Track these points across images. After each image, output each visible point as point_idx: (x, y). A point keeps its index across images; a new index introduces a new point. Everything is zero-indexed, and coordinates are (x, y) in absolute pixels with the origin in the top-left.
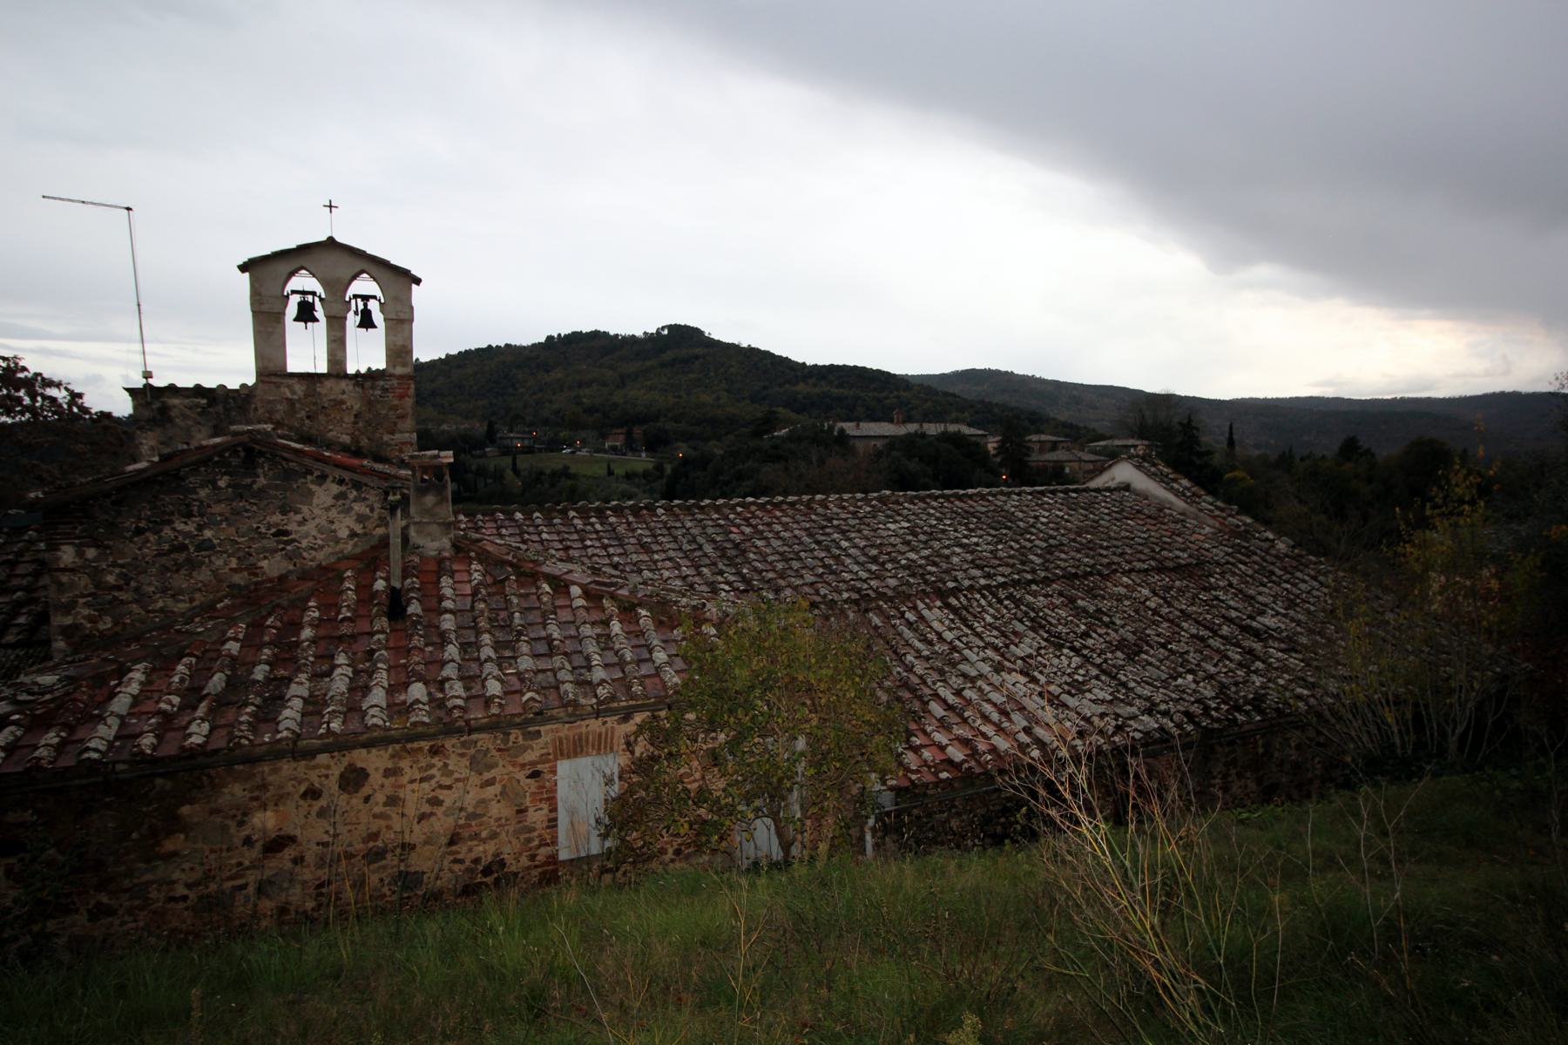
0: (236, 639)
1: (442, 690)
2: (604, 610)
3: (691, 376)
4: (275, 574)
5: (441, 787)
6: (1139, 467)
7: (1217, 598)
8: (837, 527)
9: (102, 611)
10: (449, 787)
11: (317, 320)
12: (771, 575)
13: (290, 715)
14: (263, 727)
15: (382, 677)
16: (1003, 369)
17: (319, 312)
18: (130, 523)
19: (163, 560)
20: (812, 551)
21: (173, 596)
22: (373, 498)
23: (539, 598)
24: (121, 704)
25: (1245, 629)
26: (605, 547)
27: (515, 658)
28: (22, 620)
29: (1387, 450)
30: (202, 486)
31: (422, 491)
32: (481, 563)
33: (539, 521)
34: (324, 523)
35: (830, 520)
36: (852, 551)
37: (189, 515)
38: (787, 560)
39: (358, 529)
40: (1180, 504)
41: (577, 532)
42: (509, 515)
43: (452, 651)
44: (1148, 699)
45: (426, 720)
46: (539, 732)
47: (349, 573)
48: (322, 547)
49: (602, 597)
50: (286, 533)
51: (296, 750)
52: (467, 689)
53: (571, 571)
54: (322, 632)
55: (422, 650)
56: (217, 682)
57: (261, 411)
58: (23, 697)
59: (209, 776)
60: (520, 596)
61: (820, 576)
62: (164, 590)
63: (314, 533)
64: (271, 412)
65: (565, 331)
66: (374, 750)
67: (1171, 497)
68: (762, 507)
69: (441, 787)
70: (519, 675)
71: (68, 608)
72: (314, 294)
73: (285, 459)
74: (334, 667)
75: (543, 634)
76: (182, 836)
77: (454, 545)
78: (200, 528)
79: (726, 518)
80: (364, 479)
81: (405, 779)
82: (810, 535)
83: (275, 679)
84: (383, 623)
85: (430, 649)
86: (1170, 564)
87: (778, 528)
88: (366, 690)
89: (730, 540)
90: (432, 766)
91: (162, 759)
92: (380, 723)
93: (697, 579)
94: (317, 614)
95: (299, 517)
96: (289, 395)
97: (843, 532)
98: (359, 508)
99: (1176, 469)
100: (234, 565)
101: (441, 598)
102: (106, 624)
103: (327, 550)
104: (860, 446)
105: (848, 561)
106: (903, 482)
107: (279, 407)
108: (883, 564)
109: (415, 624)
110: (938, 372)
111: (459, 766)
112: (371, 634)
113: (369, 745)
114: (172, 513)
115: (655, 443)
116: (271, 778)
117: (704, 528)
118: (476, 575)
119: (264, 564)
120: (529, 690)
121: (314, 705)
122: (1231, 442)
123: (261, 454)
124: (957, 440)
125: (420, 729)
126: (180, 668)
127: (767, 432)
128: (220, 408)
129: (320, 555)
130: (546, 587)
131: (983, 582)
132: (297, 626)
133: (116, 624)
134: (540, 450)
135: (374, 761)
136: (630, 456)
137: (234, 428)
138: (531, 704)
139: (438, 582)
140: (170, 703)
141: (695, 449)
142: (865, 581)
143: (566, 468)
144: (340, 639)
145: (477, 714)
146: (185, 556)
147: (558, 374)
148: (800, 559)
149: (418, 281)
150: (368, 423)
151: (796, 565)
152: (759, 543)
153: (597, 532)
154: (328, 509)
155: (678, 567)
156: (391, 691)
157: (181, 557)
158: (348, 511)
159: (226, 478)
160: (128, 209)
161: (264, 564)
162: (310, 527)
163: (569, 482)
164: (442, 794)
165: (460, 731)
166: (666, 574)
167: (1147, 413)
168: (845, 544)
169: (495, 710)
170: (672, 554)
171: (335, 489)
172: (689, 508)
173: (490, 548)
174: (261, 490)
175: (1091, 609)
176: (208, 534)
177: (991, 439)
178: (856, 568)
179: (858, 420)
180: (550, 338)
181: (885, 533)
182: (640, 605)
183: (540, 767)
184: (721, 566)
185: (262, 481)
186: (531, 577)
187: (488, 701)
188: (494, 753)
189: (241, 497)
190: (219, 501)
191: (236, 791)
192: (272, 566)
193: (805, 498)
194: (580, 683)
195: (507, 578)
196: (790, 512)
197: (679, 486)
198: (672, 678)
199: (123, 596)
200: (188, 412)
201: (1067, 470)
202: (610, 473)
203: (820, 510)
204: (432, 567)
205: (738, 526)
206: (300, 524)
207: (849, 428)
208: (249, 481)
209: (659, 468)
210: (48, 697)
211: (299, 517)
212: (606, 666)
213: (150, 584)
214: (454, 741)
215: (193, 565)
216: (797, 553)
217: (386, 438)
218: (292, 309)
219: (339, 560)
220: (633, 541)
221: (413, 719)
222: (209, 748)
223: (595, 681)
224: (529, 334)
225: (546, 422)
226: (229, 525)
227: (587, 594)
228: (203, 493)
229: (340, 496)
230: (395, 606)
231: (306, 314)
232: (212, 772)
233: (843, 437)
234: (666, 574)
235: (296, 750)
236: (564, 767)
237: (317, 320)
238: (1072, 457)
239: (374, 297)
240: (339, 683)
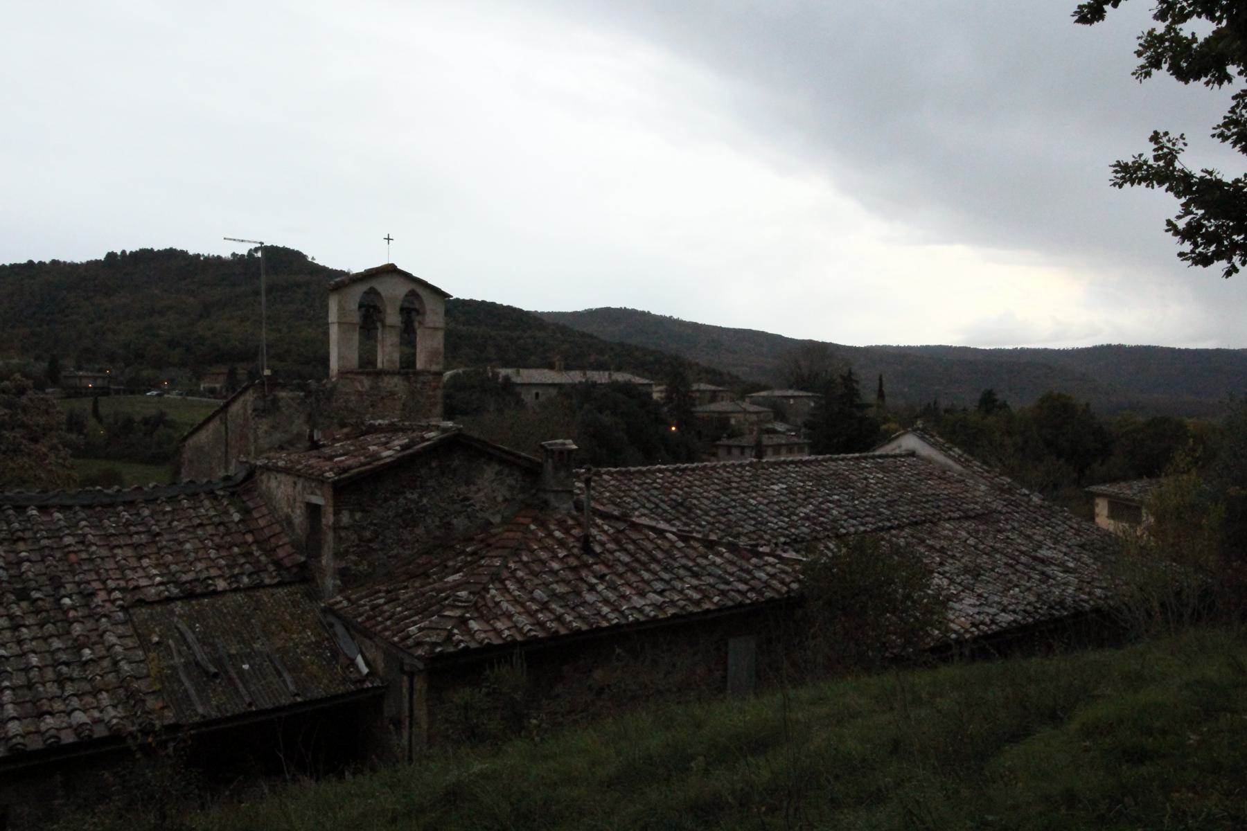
6: (922, 438)
7: (1008, 538)
16: (640, 308)
25: (1035, 558)
29: (1021, 403)
39: (508, 496)
40: (958, 467)
44: (999, 603)
50: (467, 499)
65: (132, 247)
67: (950, 462)
78: (420, 497)
86: (972, 514)
99: (950, 440)
104: (528, 397)
119: (455, 521)
122: (881, 394)
124: (627, 389)
128: (313, 399)
131: (862, 528)
143: (162, 414)
167: (802, 363)
175: (938, 546)
177: (655, 389)
180: (111, 256)
201: (733, 421)
224: (83, 248)
233: (508, 385)
238: (738, 409)
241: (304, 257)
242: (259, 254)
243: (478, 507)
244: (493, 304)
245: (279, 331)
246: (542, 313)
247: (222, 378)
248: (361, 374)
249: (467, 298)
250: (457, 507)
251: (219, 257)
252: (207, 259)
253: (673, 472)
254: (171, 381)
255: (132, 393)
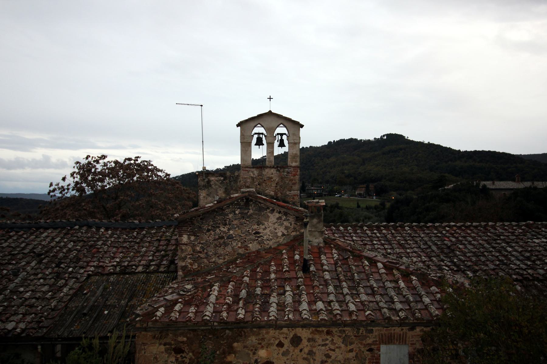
0: (247, 276)
1: (330, 306)
2: (394, 275)
3: (399, 159)
4: (254, 250)
5: (331, 350)
8: (504, 240)
9: (195, 261)
10: (334, 350)
11: (263, 145)
12: (469, 263)
13: (273, 309)
14: (263, 314)
15: (304, 297)
17: (264, 142)
18: (205, 227)
19: (216, 242)
20: (491, 252)
21: (218, 257)
22: (292, 219)
23: (363, 267)
24: (212, 299)
26: (383, 245)
27: (359, 295)
28: (164, 262)
30: (230, 213)
31: (312, 217)
32: (336, 250)
33: (351, 231)
34: (273, 229)
35: (499, 236)
36: (514, 253)
37: (225, 225)
38: (477, 256)
39: (285, 232)
41: (369, 237)
42: (337, 228)
43: (331, 288)
45: (326, 318)
46: (372, 330)
47: (284, 251)
48: (271, 240)
49: (392, 269)
50: (259, 233)
51: (276, 326)
52: (341, 306)
53: (377, 256)
54: (278, 276)
55: (318, 287)
56: (243, 293)
57: (242, 182)
58: (182, 293)
59: (244, 332)
60: (355, 266)
61: (498, 265)
62: (215, 254)
63: (269, 233)
64: (245, 182)
65: (337, 139)
66: (304, 329)
68: (459, 228)
69: (331, 350)
70: (362, 302)
71: (184, 259)
72: (262, 134)
73: (260, 203)
74: (285, 291)
75: (368, 284)
76: (234, 355)
77: (324, 241)
78: (229, 230)
79: (441, 233)
80: (289, 212)
81: (317, 344)
82: (489, 243)
83: (264, 294)
84: (300, 274)
85: (321, 287)
87: (470, 239)
88: (300, 303)
89: (445, 244)
90: (327, 339)
91: (229, 322)
92: (308, 317)
93: (430, 263)
94: (275, 268)
95: (263, 227)
96: (252, 175)
97: (507, 243)
98: (286, 223)
100: (240, 246)
101: (323, 265)
102: (195, 266)
103: (273, 241)
105: (513, 259)
106: (521, 215)
107: (248, 180)
108: (534, 261)
109: (314, 275)
110: (541, 153)
111: (339, 341)
112: (297, 278)
113: (304, 326)
114: (220, 224)
115: (380, 192)
116: (266, 336)
117: (430, 237)
118: (335, 255)
119: (250, 245)
120: (368, 310)
121: (281, 307)
123: (251, 200)
125: (323, 322)
126: (230, 286)
127: (440, 187)
128: (228, 181)
129: (271, 243)
130: (366, 263)
132: (268, 272)
133: (199, 267)
134: (325, 195)
135: (304, 334)
136: (368, 198)
137: (242, 190)
138: (370, 316)
139: (320, 258)
140: (229, 300)
141: (400, 195)
142: (525, 270)
143: (337, 204)
144: (286, 279)
145: (347, 318)
146: (223, 241)
147: (333, 159)
148: (484, 256)
149: (302, 126)
150: (281, 187)
151: (483, 259)
152: (461, 246)
153: (378, 237)
154: (274, 224)
155: (420, 256)
156: (310, 303)
157: (222, 241)
158: (282, 225)
159: (239, 210)
160: (202, 106)
161: (250, 245)
162: (267, 231)
163: (340, 211)
164: (331, 353)
165: (339, 325)
166: (415, 259)
168: (509, 249)
169: (354, 317)
170: (416, 249)
171: (278, 215)
172: (421, 227)
173: (339, 243)
174: (251, 215)
176: (231, 232)
178: (518, 263)
179: (492, 180)
180: (330, 143)
181: (533, 245)
182: (412, 273)
183: (373, 347)
184: (442, 257)
185: (251, 211)
186: (359, 257)
187: (351, 313)
188: (353, 337)
189: (243, 218)
190: (236, 219)
191: (253, 340)
192: (253, 247)
193: (483, 224)
194: (390, 309)
195: (349, 257)
196: (475, 231)
197: (394, 215)
198: (434, 311)
199: (202, 255)
200: (217, 183)
202: (359, 206)
203: (492, 230)
204: (316, 250)
205: (448, 237)
206: (264, 229)
207: (489, 184)
208: (246, 211)
209: (383, 204)
210: (189, 293)
211: (263, 227)
212: (401, 302)
213: (211, 251)
214: (336, 329)
215: (226, 244)
216: (483, 253)
217: (288, 193)
218: (254, 141)
219: (278, 245)
220: (395, 242)
221: (321, 317)
222: (246, 320)
223: (398, 309)
225: (327, 182)
226: (239, 229)
227: (385, 266)
228: (231, 216)
229: (279, 218)
230: (305, 268)
231: (259, 142)
232: (245, 330)
234: (415, 259)
235: (276, 326)
236: (383, 348)
237: (263, 145)
239: (285, 134)
240: (289, 298)
241: (404, 137)
242: (385, 138)
243: (265, 238)
244: (495, 152)
245: (392, 169)
246: (524, 155)
247: (364, 189)
248: (253, 168)
249: (481, 150)
250: (253, 237)
251: (369, 140)
252: (365, 141)
253: (459, 228)
254: (345, 191)
255: (330, 195)
